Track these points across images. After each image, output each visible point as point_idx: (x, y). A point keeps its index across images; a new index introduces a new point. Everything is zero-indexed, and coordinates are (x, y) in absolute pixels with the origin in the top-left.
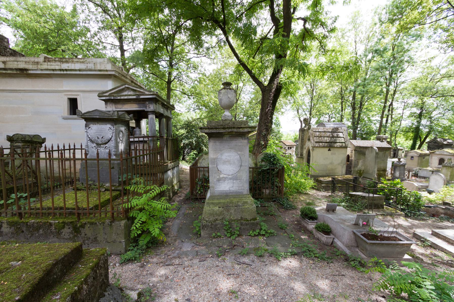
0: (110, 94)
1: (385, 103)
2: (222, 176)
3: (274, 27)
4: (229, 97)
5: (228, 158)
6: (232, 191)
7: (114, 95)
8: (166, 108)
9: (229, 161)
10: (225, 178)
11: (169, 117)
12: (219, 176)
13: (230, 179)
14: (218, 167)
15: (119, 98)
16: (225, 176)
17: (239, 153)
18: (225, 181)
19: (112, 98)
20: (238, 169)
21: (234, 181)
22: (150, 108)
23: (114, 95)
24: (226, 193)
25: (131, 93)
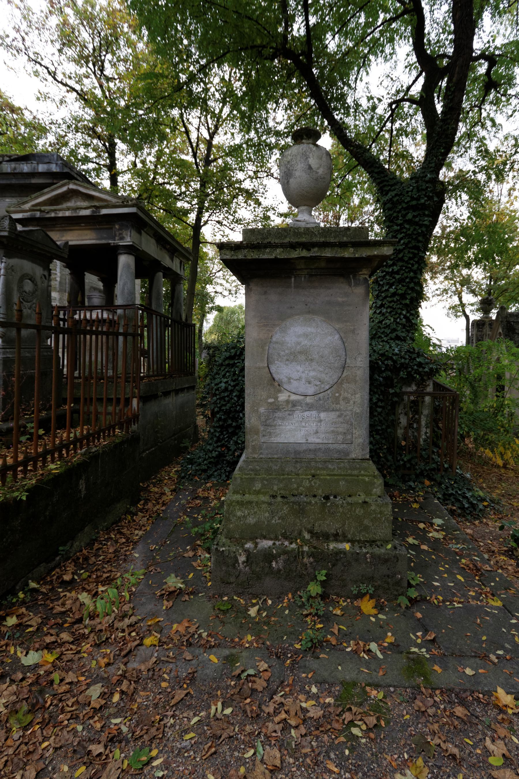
0: (33, 206)
1: (170, 662)
2: (283, 397)
3: (424, 74)
4: (310, 168)
5: (305, 342)
6: (312, 447)
7: (43, 208)
8: (168, 251)
9: (305, 352)
10: (294, 404)
11: (178, 275)
12: (276, 398)
13: (310, 407)
14: (273, 369)
15: (53, 215)
16: (293, 397)
17: (337, 326)
18: (292, 412)
19: (38, 214)
20: (335, 377)
21: (323, 415)
22: (122, 238)
23: (43, 208)
24: (297, 452)
25: (85, 204)
